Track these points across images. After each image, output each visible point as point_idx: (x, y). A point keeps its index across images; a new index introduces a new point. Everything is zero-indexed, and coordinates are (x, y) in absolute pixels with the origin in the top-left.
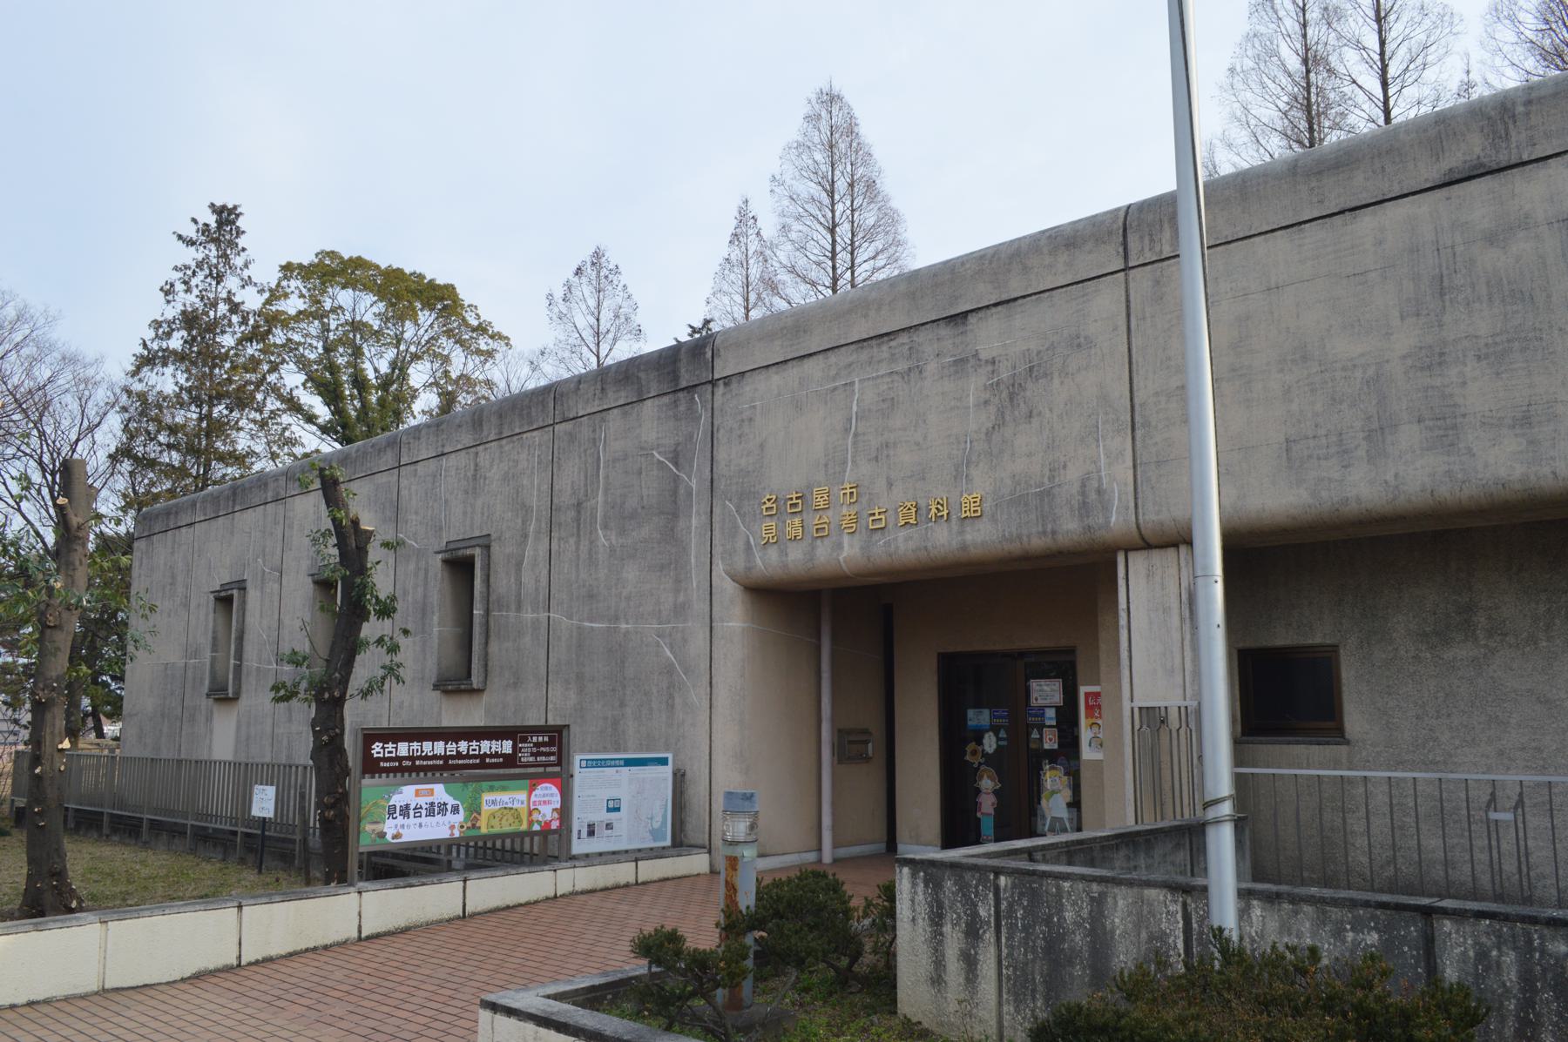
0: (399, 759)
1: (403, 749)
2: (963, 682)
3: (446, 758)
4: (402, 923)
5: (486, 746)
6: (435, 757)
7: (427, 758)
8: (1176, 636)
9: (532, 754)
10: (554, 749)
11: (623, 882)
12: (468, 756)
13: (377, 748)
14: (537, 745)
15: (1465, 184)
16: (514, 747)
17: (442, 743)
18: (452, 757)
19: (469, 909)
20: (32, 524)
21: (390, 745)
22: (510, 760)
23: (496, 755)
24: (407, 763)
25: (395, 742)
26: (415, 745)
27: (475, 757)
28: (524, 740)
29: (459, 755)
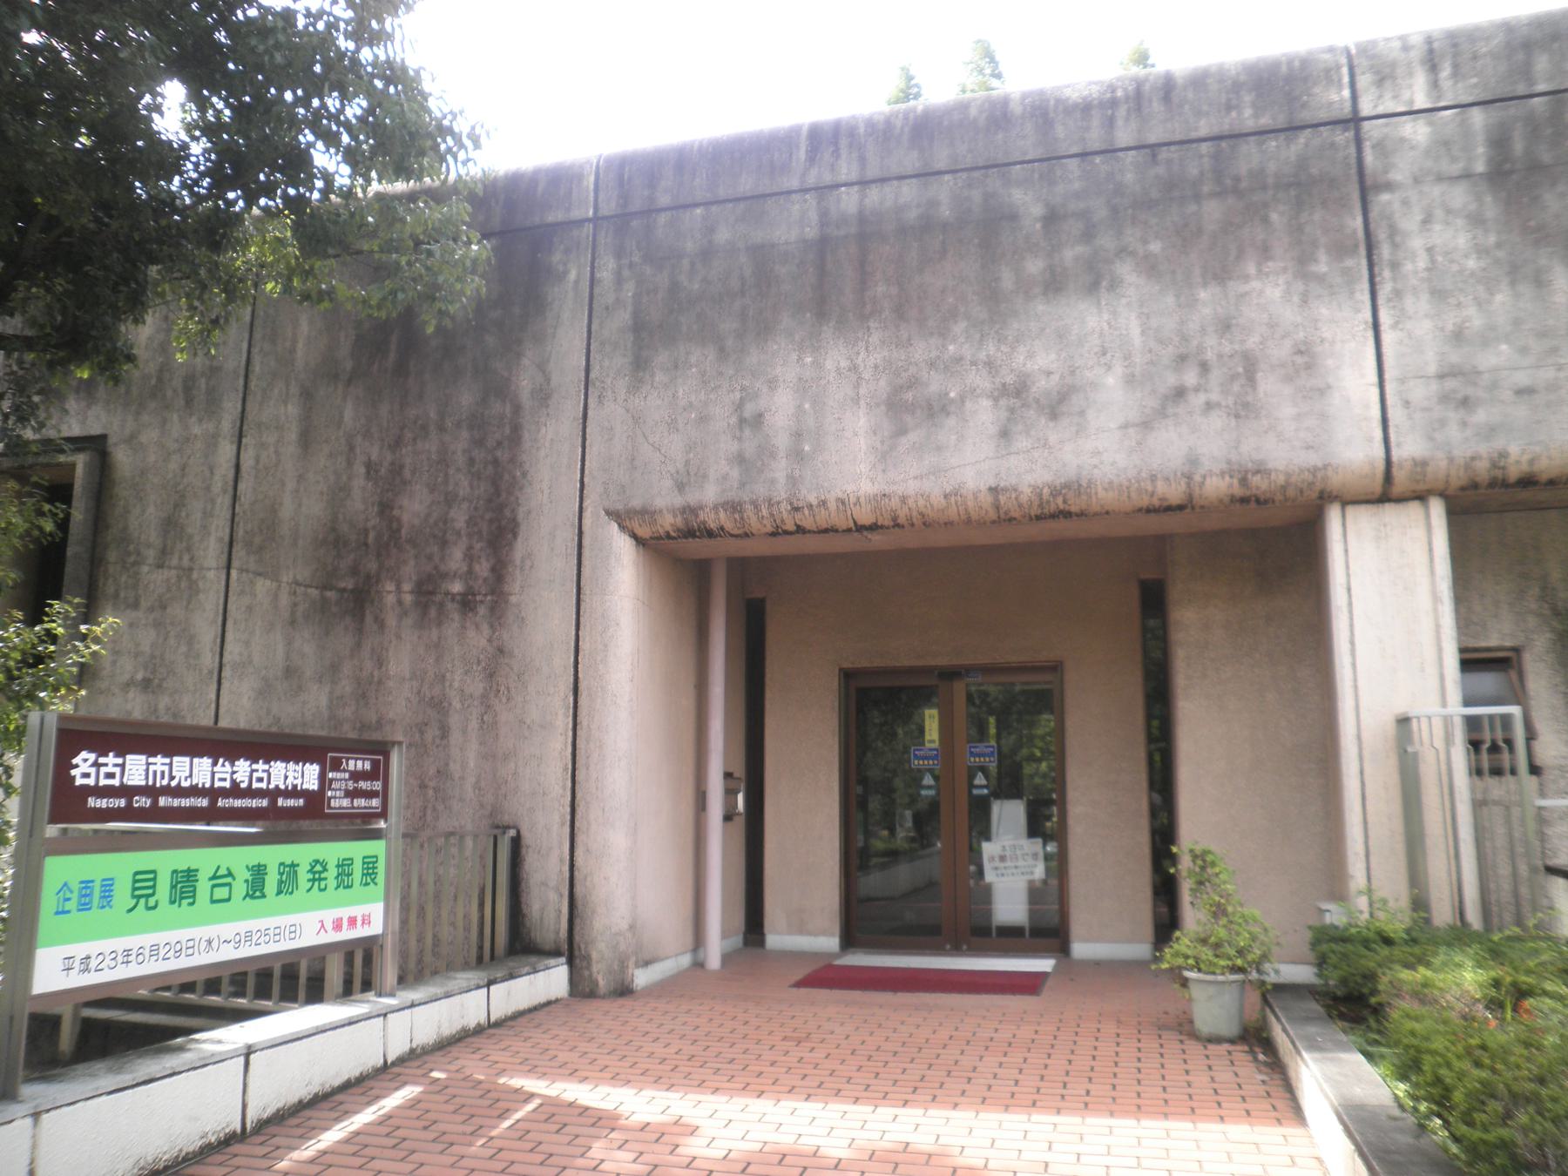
0: (127, 791)
1: (136, 769)
2: (875, 708)
3: (213, 793)
4: (543, 1000)
5: (281, 774)
6: (194, 791)
7: (179, 792)
8: (1427, 624)
9: (351, 794)
10: (377, 786)
11: (472, 1025)
12: (250, 793)
13: (84, 767)
14: (356, 776)
15: (1360, 693)
16: (322, 776)
17: (206, 762)
18: (224, 793)
19: (493, 1019)
20: (4, 239)
21: (111, 759)
22: (315, 802)
23: (294, 793)
24: (142, 802)
25: (121, 753)
26: (159, 762)
27: (260, 793)
28: (336, 766)
29: (235, 791)
